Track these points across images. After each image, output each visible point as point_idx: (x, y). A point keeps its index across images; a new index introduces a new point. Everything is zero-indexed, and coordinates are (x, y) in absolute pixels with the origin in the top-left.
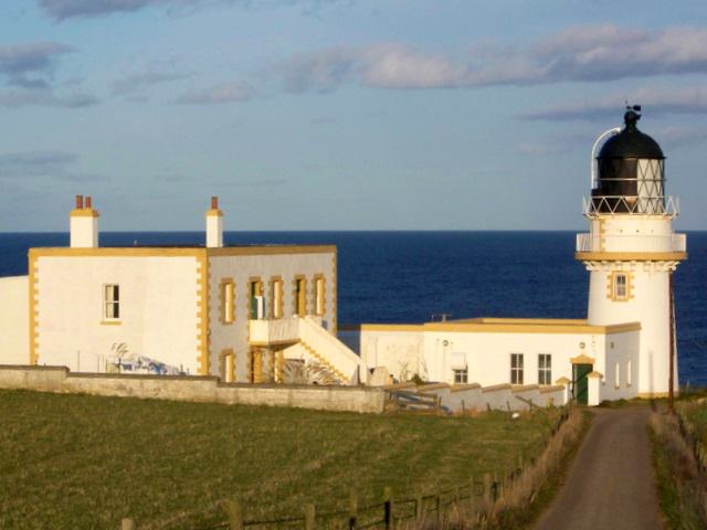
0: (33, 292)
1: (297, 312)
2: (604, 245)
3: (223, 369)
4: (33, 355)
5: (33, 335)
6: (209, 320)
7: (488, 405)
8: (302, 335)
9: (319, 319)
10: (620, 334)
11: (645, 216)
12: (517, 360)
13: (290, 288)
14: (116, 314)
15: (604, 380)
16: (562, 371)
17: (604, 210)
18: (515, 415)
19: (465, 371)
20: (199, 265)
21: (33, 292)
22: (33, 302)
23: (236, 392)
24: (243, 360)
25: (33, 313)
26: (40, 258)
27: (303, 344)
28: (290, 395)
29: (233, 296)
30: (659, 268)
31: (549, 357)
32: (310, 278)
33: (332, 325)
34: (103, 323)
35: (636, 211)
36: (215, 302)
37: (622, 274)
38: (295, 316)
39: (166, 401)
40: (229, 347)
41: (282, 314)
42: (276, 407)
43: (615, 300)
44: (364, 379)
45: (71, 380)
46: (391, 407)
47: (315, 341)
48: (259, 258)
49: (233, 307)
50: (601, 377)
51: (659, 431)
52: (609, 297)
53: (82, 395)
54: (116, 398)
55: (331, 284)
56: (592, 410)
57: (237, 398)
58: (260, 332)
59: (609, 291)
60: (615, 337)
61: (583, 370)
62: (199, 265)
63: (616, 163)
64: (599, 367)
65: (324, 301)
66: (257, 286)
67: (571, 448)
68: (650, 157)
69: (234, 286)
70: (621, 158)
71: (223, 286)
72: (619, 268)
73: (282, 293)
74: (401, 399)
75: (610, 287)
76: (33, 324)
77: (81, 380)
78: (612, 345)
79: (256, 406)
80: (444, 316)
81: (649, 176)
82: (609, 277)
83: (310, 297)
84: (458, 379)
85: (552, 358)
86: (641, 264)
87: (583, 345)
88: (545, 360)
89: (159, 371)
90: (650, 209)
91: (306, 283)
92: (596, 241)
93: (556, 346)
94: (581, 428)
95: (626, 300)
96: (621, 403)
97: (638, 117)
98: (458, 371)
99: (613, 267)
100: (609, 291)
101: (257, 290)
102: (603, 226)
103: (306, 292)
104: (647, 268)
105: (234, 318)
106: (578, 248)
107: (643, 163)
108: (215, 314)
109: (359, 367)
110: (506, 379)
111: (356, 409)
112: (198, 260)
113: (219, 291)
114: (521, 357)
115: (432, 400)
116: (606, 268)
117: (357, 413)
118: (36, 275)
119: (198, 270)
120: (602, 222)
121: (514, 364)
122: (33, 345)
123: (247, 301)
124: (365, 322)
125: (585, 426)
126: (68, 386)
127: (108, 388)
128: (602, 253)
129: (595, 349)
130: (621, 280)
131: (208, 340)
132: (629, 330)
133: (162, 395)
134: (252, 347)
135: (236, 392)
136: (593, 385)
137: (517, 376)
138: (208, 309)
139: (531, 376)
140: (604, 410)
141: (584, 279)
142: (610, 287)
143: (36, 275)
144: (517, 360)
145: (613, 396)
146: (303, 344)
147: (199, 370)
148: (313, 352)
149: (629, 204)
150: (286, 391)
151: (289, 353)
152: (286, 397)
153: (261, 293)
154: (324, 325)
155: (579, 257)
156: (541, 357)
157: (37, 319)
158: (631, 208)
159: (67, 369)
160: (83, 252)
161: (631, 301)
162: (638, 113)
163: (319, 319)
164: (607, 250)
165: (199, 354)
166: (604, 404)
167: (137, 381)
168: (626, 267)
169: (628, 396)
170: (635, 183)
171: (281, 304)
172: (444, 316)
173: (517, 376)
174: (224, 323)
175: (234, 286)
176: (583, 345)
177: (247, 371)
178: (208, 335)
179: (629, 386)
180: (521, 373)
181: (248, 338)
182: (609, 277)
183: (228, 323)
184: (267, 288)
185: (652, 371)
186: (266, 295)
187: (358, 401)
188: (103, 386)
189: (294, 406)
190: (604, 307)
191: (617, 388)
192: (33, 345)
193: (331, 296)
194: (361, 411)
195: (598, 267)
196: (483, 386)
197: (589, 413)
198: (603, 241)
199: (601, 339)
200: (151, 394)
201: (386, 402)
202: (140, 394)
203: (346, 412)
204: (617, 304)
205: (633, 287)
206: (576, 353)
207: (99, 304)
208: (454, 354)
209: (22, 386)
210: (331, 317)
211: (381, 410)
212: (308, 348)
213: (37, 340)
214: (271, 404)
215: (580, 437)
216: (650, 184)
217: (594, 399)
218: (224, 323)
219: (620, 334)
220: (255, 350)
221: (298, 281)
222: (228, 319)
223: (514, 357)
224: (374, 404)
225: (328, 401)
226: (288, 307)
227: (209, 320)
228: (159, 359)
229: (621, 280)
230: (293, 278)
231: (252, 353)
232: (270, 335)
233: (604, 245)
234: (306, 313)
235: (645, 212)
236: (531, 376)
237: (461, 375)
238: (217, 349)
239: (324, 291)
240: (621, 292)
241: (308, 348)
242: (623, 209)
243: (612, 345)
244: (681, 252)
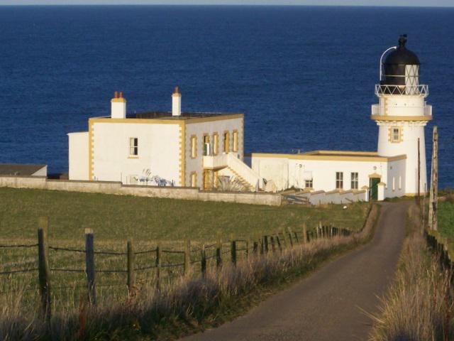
0: (91, 141)
1: (225, 151)
2: (387, 112)
3: (191, 182)
4: (91, 174)
5: (91, 163)
6: (185, 157)
7: (320, 201)
8: (228, 163)
9: (236, 154)
10: (396, 162)
11: (409, 97)
12: (339, 175)
13: (221, 138)
14: (136, 152)
15: (386, 187)
16: (364, 182)
17: (387, 92)
18: (345, 207)
19: (311, 181)
20: (181, 129)
21: (91, 141)
22: (91, 147)
23: (208, 195)
24: (200, 177)
25: (91, 152)
26: (95, 124)
27: (229, 168)
28: (235, 196)
29: (196, 144)
30: (416, 124)
31: (357, 174)
32: (231, 132)
33: (241, 157)
34: (129, 158)
35: (404, 93)
36: (188, 148)
37: (396, 128)
38: (224, 153)
39: (173, 199)
40: (194, 170)
41: (218, 152)
42: (228, 202)
43: (393, 142)
44: (261, 187)
45: (124, 188)
46: (285, 203)
47: (233, 165)
48: (196, 125)
49: (196, 150)
50: (385, 185)
51: (410, 216)
52: (389, 140)
53: (129, 196)
54: (148, 198)
55: (241, 135)
56: (381, 203)
57: (208, 198)
58: (209, 162)
59: (389, 138)
60: (393, 164)
61: (375, 181)
62: (181, 129)
63: (394, 67)
64: (384, 180)
65: (238, 144)
66: (206, 138)
67: (375, 222)
68: (412, 64)
69: (196, 139)
70: (397, 64)
71: (213, 136)
72: (395, 125)
73: (218, 141)
74: (289, 199)
75: (390, 135)
76: (91, 157)
77: (129, 188)
78: (391, 168)
79: (218, 202)
80: (299, 151)
81: (412, 74)
82: (390, 130)
83: (231, 142)
84: (307, 185)
85: (359, 175)
86: (407, 123)
87: (375, 168)
88: (354, 175)
89: (162, 184)
90: (412, 92)
91: (229, 135)
92: (383, 109)
93: (362, 168)
94: (378, 216)
95: (398, 142)
96: (396, 199)
97: (405, 41)
98: (307, 181)
99: (392, 124)
100: (389, 138)
101: (206, 140)
102: (387, 101)
103: (229, 140)
104: (410, 125)
105: (196, 155)
106: (373, 113)
107: (408, 67)
108: (188, 154)
109: (259, 181)
110: (333, 187)
111: (267, 204)
112: (180, 126)
113: (190, 142)
114: (342, 173)
115: (305, 200)
116: (388, 124)
117: (268, 206)
118: (93, 132)
119: (180, 131)
120: (386, 99)
121: (338, 177)
122: (91, 169)
123: (202, 146)
124: (255, 152)
125: (379, 212)
126: (122, 192)
127: (143, 192)
128: (386, 116)
129: (382, 170)
130: (396, 131)
131: (185, 167)
132: (395, 160)
133: (170, 196)
134: (205, 170)
135: (208, 195)
136: (381, 189)
137: (339, 184)
138: (185, 151)
139: (347, 186)
140: (388, 203)
141: (375, 130)
142: (390, 135)
143: (93, 132)
144: (339, 175)
145: (391, 196)
146: (229, 168)
147: (180, 183)
148: (234, 172)
149: (400, 89)
150: (233, 195)
151: (221, 173)
152: (233, 197)
153: (209, 141)
154: (239, 157)
155: (373, 118)
156: (353, 174)
157: (93, 155)
158: (403, 92)
159: (121, 183)
160: (118, 121)
161: (401, 143)
162: (405, 38)
163: (236, 154)
164: (389, 115)
165: (180, 174)
166: (386, 200)
167: (158, 189)
168: (399, 124)
169: (399, 195)
170: (404, 78)
171: (218, 147)
172: (299, 151)
173: (339, 184)
174: (192, 158)
175: (196, 139)
176: (375, 168)
177: (202, 183)
178: (185, 165)
179: (399, 189)
180: (342, 182)
181: (202, 166)
182: (390, 130)
183: (194, 158)
184: (211, 139)
185: (411, 182)
186: (211, 142)
187: (269, 200)
188: (140, 192)
189: (237, 202)
190: (387, 146)
191: (393, 191)
192: (91, 169)
193: (241, 141)
194: (270, 205)
195: (383, 124)
196: (326, 191)
197: (379, 205)
198: (386, 110)
199: (385, 164)
200: (165, 196)
201: (282, 201)
202: (159, 195)
203: (263, 206)
204: (393, 144)
205: (402, 135)
206: (371, 172)
207: (128, 148)
208: (305, 172)
209: (98, 191)
210: (241, 152)
211: (280, 204)
212: (232, 170)
213: (93, 166)
214: (225, 201)
215: (377, 218)
216: (412, 78)
217: (381, 197)
218: (192, 158)
219: (396, 162)
220: (206, 171)
221: (225, 135)
222: (193, 156)
223: (338, 174)
224: (277, 201)
225: (254, 200)
226: (221, 148)
227: (185, 157)
228: (162, 177)
229: (396, 131)
230: (223, 133)
231: (204, 173)
232: (214, 163)
233: (387, 112)
234: (229, 151)
235: (409, 94)
236: (347, 186)
237: (309, 184)
238: (189, 171)
239: (237, 138)
240: (396, 138)
241: (232, 170)
242: (397, 92)
243: (391, 168)
244: (429, 116)
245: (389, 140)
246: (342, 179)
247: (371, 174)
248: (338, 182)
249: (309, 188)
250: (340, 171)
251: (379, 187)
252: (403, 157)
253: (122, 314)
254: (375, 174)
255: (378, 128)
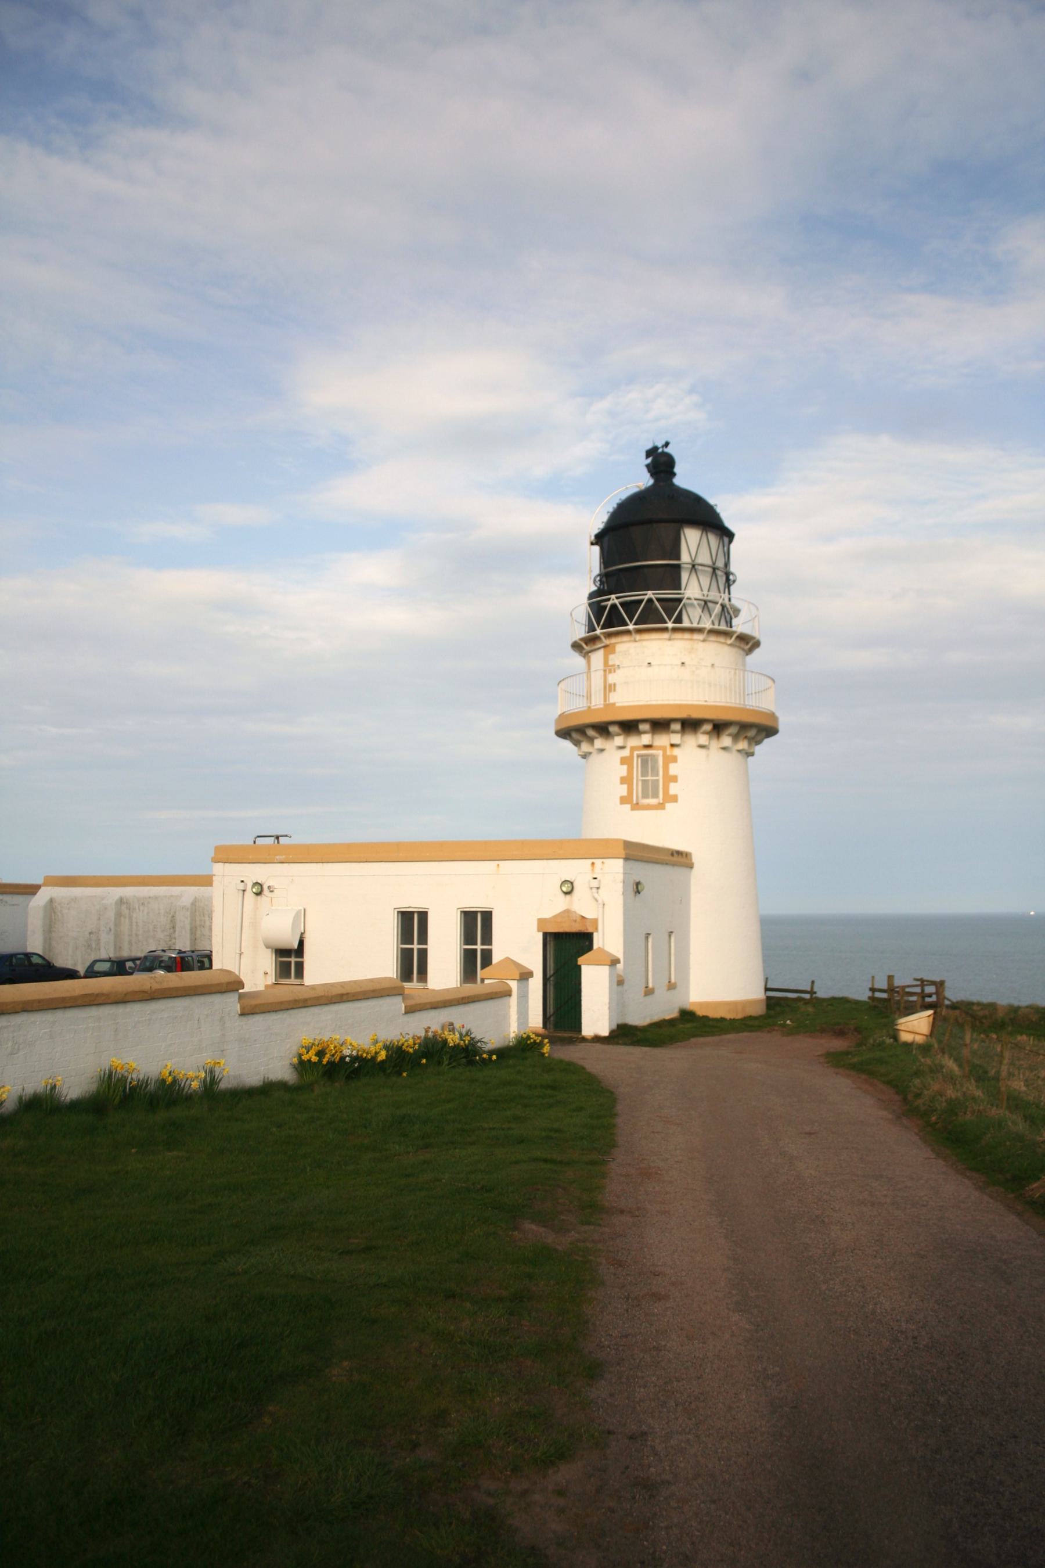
7: (890, 978)
12: (413, 925)
16: (518, 945)
19: (300, 951)
43: (636, 807)
50: (614, 962)
59: (623, 790)
61: (567, 949)
64: (609, 938)
75: (626, 780)
87: (569, 888)
88: (477, 925)
95: (661, 806)
100: (623, 790)
110: (385, 965)
114: (423, 916)
116: (619, 740)
121: (406, 935)
137: (413, 964)
139: (444, 969)
142: (626, 780)
144: (413, 925)
145: (640, 1017)
170: (678, 567)
173: (413, 964)
176: (569, 888)
180: (423, 954)
206: (552, 907)
217: (596, 1017)
236: (444, 969)
243: (638, 889)
245: (624, 800)
246: (423, 938)
247: (548, 914)
248: (406, 957)
249: (293, 980)
250: (413, 903)
251: (585, 970)
252: (680, 859)
253: (444, 1067)
254: (567, 912)
255: (579, 967)
